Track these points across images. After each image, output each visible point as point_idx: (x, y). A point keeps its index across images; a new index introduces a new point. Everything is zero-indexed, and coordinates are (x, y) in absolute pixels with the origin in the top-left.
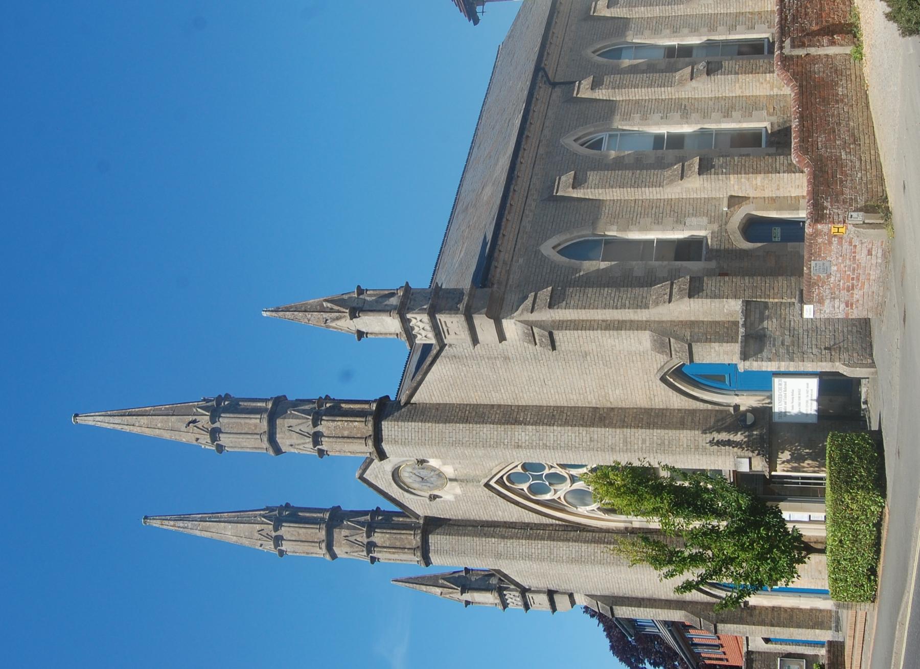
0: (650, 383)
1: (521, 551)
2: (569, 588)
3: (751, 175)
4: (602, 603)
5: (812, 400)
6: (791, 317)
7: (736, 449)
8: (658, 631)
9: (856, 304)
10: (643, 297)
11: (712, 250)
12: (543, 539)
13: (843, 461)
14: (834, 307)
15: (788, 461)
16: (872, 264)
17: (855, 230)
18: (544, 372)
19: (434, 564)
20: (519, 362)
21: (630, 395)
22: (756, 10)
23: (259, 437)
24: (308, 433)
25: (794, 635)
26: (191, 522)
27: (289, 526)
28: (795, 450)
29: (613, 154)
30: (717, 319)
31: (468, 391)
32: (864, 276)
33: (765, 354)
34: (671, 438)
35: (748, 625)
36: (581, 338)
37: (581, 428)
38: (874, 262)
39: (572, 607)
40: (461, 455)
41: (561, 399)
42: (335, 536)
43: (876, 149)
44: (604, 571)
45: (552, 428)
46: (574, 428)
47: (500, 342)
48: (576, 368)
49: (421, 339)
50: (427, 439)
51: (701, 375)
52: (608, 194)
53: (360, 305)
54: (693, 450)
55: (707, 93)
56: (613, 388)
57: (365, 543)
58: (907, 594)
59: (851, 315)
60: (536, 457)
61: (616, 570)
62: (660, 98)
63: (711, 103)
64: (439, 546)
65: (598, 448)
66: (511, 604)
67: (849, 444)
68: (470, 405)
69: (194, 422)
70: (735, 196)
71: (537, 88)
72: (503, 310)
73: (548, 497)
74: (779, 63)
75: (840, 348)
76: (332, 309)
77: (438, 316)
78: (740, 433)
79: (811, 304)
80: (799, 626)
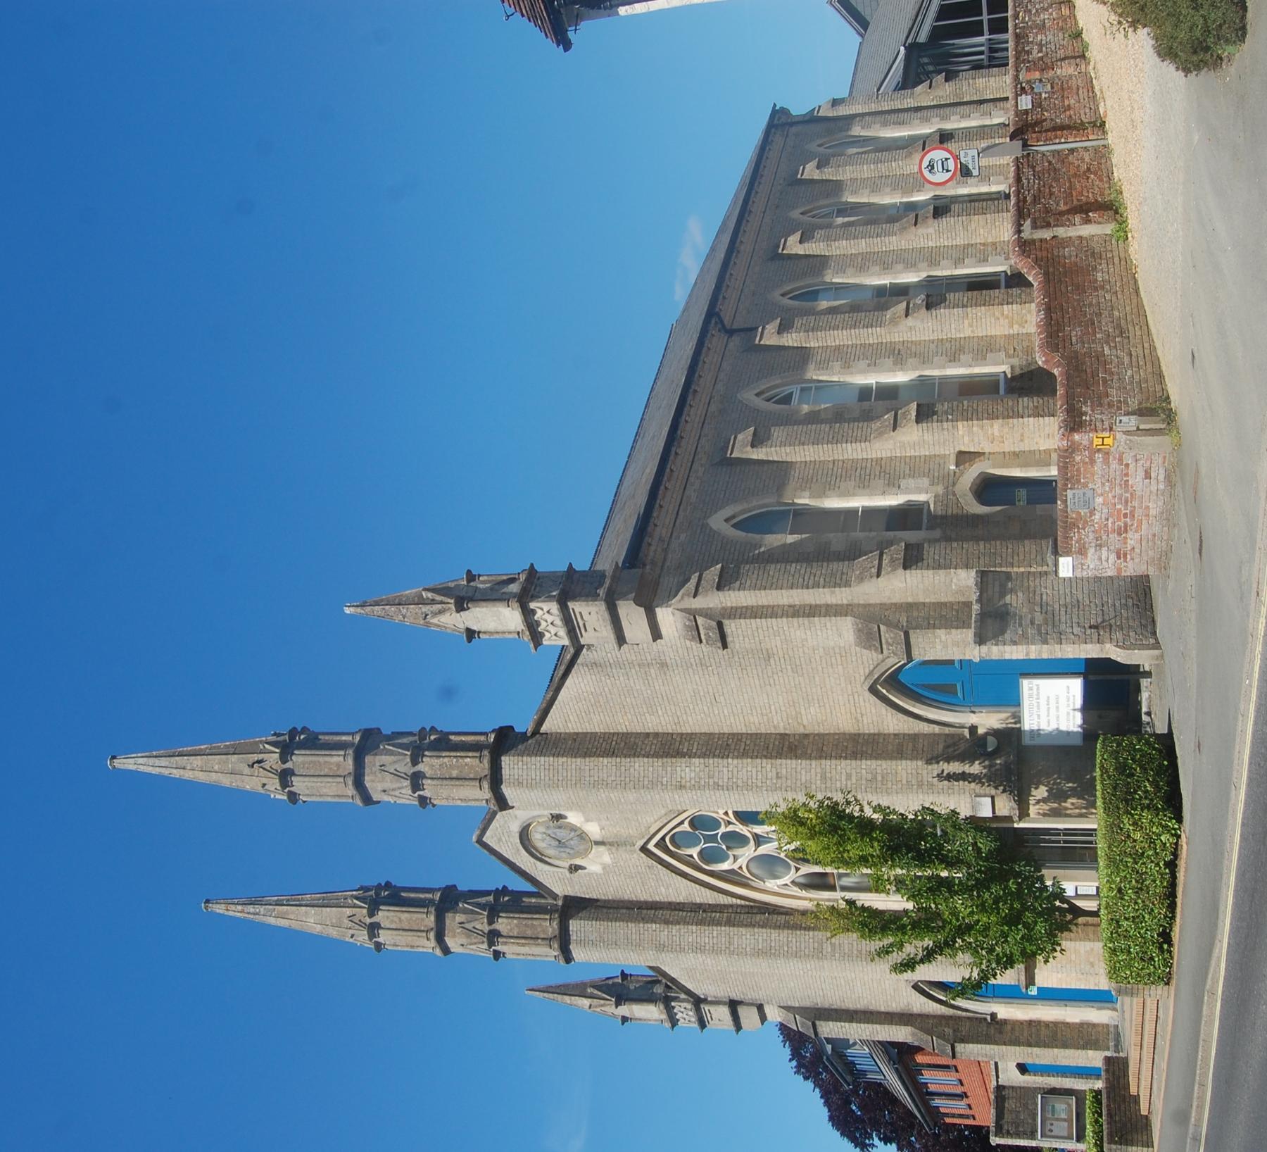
0: (856, 696)
1: (690, 940)
2: (757, 997)
5: (1074, 710)
7: (973, 784)
8: (883, 1077)
9: (1130, 554)
10: (842, 573)
11: (936, 517)
12: (719, 924)
13: (1120, 773)
14: (1100, 559)
15: (1044, 800)
16: (1151, 492)
17: (1127, 440)
20: (681, 669)
23: (342, 780)
24: (405, 774)
25: (1060, 1059)
28: (1053, 784)
29: (806, 408)
33: (1008, 636)
34: (885, 771)
35: (997, 1044)
37: (764, 761)
38: (1154, 488)
39: (762, 1024)
40: (605, 801)
41: (738, 724)
42: (448, 922)
43: (1151, 341)
44: (801, 968)
45: (725, 761)
47: (654, 641)
48: (756, 677)
49: (550, 639)
50: (560, 779)
51: (923, 685)
52: (798, 454)
53: (470, 594)
54: (915, 787)
56: (807, 705)
57: (486, 932)
59: (1125, 571)
60: (705, 801)
61: (817, 965)
62: (867, 342)
63: (933, 346)
65: (787, 787)
68: (618, 734)
69: (259, 762)
71: (709, 335)
72: (657, 597)
73: (725, 866)
74: (1017, 249)
75: (1111, 626)
76: (433, 600)
77: (571, 605)
78: (977, 762)
79: (1068, 556)
80: (1065, 1046)
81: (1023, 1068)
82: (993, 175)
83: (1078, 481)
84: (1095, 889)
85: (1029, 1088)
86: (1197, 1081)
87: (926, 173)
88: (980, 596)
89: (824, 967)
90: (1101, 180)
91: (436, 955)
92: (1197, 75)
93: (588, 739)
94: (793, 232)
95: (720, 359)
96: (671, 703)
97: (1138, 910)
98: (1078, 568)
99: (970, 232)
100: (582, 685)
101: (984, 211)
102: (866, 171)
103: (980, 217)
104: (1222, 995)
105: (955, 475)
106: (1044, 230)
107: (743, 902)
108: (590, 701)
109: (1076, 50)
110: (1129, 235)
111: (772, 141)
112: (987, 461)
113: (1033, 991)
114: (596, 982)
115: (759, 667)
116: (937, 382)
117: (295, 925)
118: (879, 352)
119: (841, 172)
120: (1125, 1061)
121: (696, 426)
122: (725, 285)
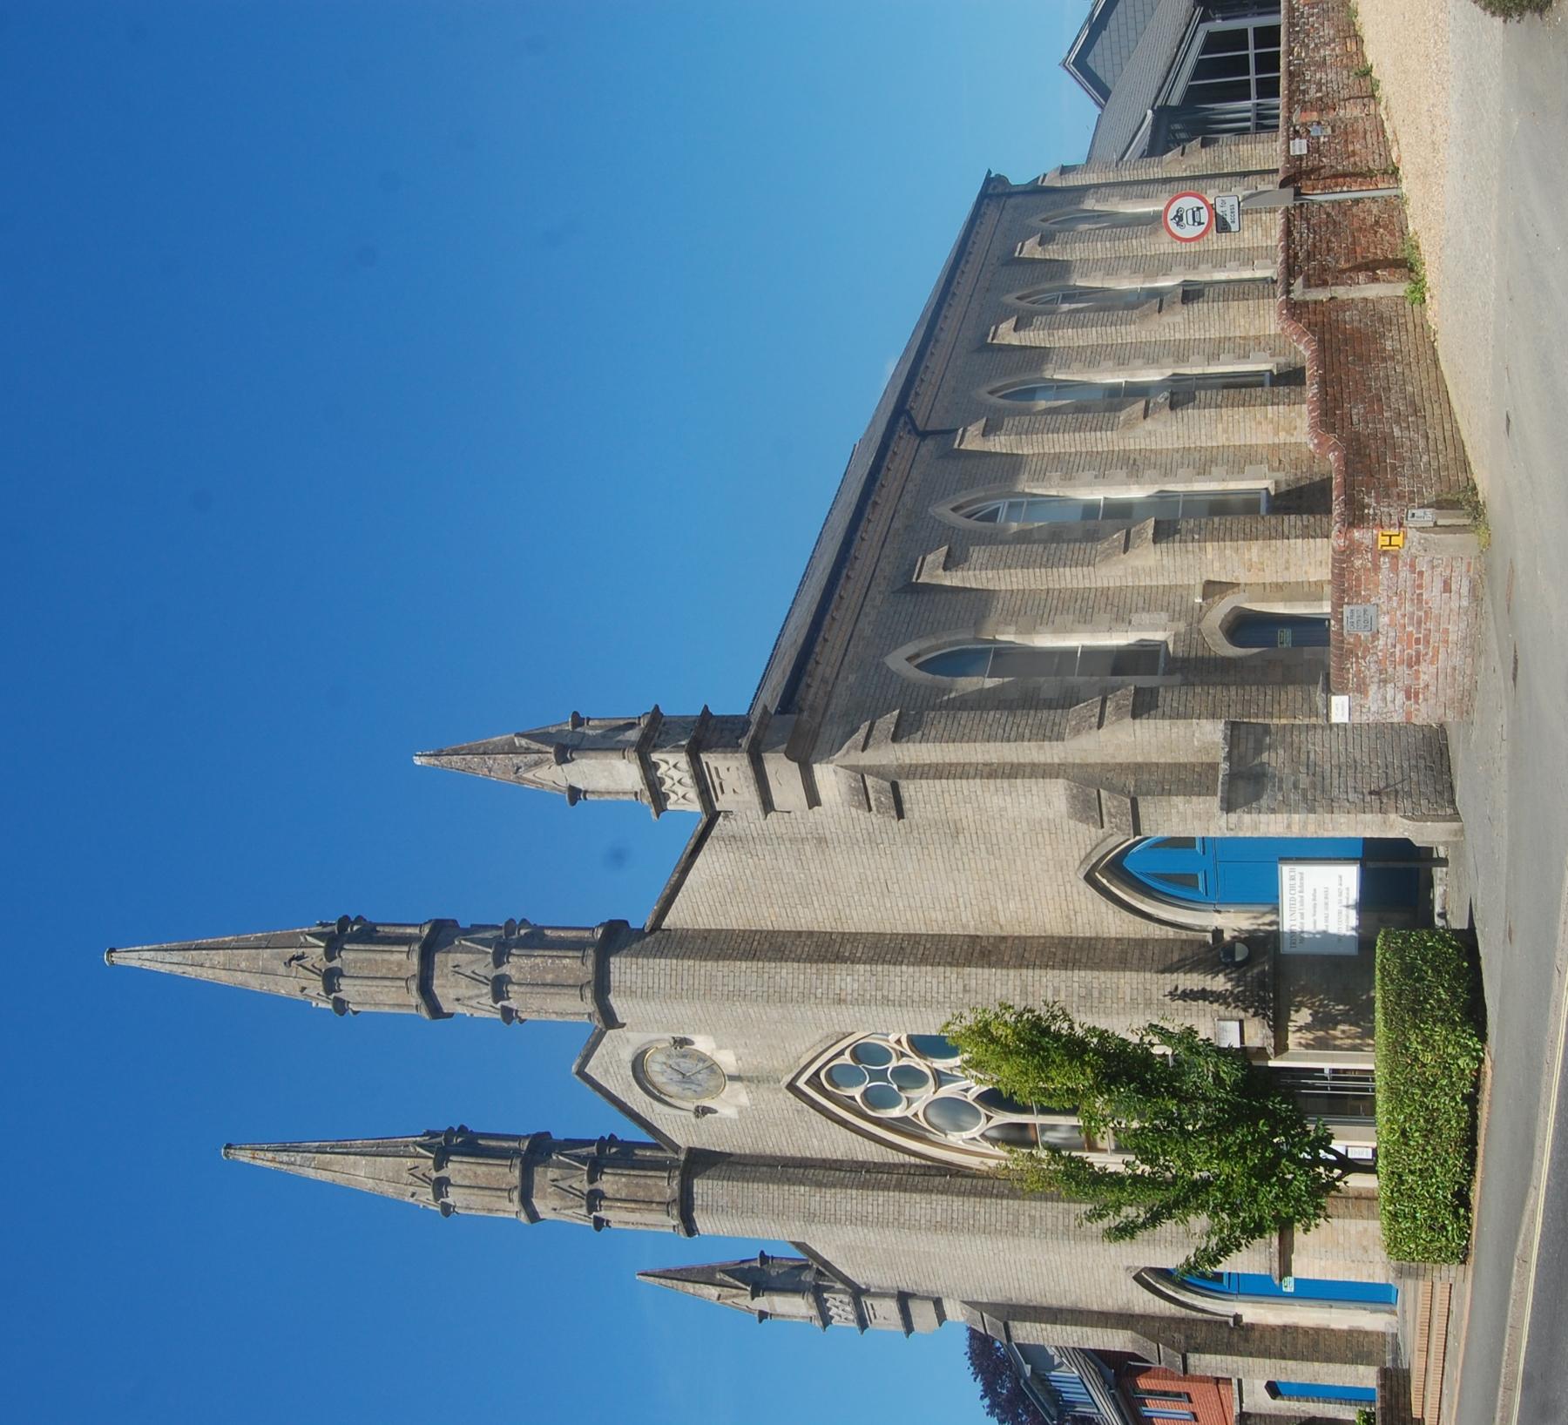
1: (848, 1208)
2: (935, 1289)
3: (1240, 543)
4: (991, 1315)
5: (1348, 907)
6: (1310, 746)
7: (1215, 1006)
8: (1096, 1411)
10: (1054, 724)
11: (1175, 659)
12: (886, 1188)
14: (1384, 699)
16: (1451, 610)
17: (1421, 538)
18: (885, 866)
19: (701, 1232)
20: (843, 847)
21: (1033, 911)
22: (1251, 334)
23: (403, 984)
24: (486, 978)
26: (301, 1154)
27: (461, 1162)
28: (1319, 1006)
29: (1014, 526)
30: (1183, 760)
31: (758, 905)
32: (1437, 634)
33: (1264, 802)
34: (1103, 985)
35: (1241, 1356)
36: (946, 795)
37: (948, 969)
38: (1454, 605)
39: (940, 1325)
40: (742, 1019)
41: (916, 921)
42: (537, 1178)
43: (1453, 421)
45: (898, 968)
46: (935, 969)
47: (810, 808)
48: (940, 858)
50: (685, 987)
55: (1170, 442)
56: (1004, 898)
57: (585, 1192)
58: (1534, 1193)
59: (1416, 716)
60: (871, 1021)
61: (1012, 1245)
62: (1095, 450)
63: (1177, 456)
64: (710, 1199)
66: (837, 1318)
67: (1416, 949)
68: (761, 932)
69: (298, 958)
70: (1214, 582)
71: (896, 437)
73: (896, 1112)
74: (1285, 312)
75: (1397, 792)
76: (528, 749)
77: (704, 757)
79: (1344, 694)
80: (1329, 1359)
81: (1273, 1389)
82: (1257, 258)
83: (1358, 594)
84: (1370, 1151)
85: (1282, 1417)
86: (1502, 1384)
87: (1172, 225)
88: (1230, 752)
89: (1020, 1249)
90: (1393, 235)
91: (521, 1222)
92: (1518, 22)
93: (723, 937)
94: (1006, 318)
95: (908, 466)
96: (830, 890)
97: (1426, 1160)
98: (1356, 711)
99: (1227, 322)
100: (717, 865)
101: (1246, 297)
102: (1101, 249)
103: (1241, 303)
104: (1538, 1260)
105: (1201, 610)
106: (1320, 289)
107: (918, 1161)
108: (726, 887)
109: (1364, 89)
110: (1427, 297)
111: (985, 213)
112: (1242, 594)
113: (1289, 1286)
114: (727, 1266)
115: (944, 846)
116: (1181, 499)
117: (340, 1179)
118: (1109, 462)
119: (1069, 251)
120: (1406, 1376)
121: (874, 544)
122: (918, 379)
